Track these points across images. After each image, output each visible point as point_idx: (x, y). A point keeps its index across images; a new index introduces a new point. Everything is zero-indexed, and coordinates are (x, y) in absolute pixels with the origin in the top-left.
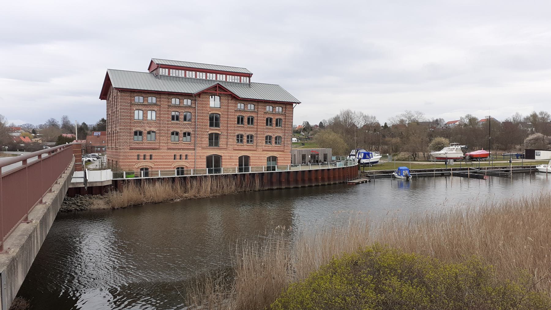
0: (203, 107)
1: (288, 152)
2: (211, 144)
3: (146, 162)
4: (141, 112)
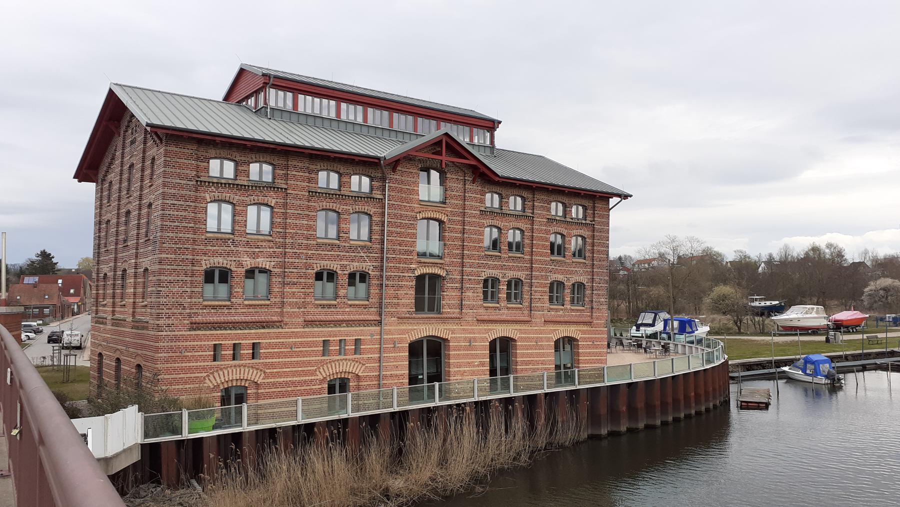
0: (402, 200)
1: (598, 325)
2: (419, 306)
3: (239, 366)
4: (227, 209)
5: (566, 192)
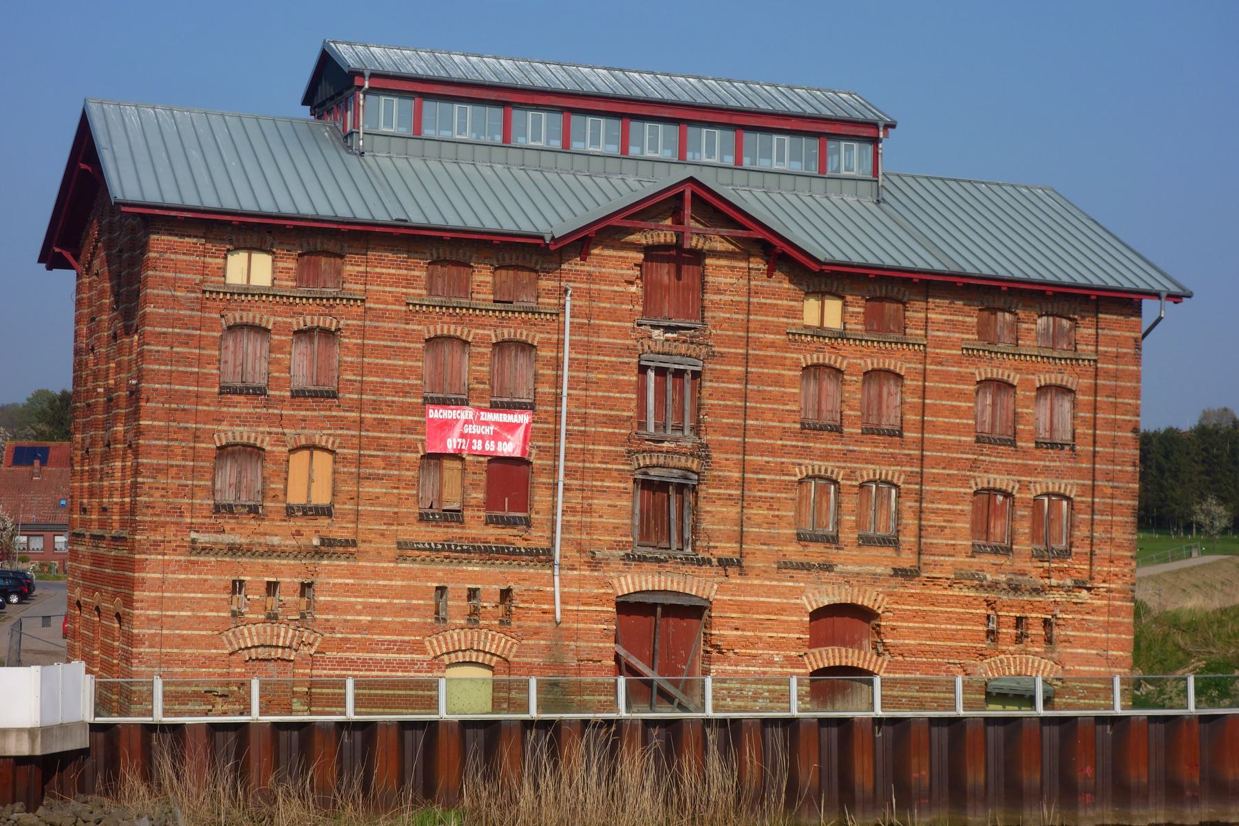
5: (1003, 289)
